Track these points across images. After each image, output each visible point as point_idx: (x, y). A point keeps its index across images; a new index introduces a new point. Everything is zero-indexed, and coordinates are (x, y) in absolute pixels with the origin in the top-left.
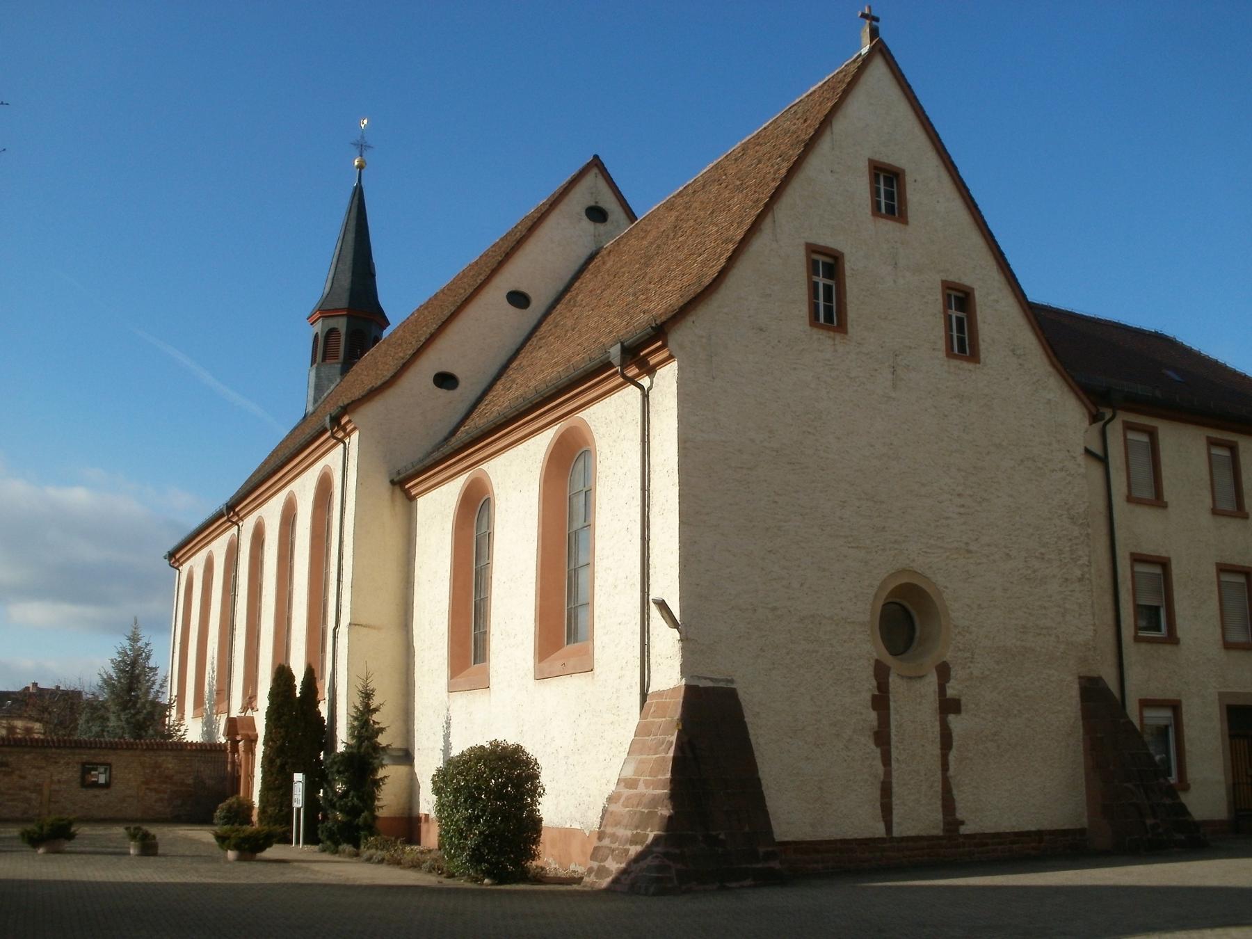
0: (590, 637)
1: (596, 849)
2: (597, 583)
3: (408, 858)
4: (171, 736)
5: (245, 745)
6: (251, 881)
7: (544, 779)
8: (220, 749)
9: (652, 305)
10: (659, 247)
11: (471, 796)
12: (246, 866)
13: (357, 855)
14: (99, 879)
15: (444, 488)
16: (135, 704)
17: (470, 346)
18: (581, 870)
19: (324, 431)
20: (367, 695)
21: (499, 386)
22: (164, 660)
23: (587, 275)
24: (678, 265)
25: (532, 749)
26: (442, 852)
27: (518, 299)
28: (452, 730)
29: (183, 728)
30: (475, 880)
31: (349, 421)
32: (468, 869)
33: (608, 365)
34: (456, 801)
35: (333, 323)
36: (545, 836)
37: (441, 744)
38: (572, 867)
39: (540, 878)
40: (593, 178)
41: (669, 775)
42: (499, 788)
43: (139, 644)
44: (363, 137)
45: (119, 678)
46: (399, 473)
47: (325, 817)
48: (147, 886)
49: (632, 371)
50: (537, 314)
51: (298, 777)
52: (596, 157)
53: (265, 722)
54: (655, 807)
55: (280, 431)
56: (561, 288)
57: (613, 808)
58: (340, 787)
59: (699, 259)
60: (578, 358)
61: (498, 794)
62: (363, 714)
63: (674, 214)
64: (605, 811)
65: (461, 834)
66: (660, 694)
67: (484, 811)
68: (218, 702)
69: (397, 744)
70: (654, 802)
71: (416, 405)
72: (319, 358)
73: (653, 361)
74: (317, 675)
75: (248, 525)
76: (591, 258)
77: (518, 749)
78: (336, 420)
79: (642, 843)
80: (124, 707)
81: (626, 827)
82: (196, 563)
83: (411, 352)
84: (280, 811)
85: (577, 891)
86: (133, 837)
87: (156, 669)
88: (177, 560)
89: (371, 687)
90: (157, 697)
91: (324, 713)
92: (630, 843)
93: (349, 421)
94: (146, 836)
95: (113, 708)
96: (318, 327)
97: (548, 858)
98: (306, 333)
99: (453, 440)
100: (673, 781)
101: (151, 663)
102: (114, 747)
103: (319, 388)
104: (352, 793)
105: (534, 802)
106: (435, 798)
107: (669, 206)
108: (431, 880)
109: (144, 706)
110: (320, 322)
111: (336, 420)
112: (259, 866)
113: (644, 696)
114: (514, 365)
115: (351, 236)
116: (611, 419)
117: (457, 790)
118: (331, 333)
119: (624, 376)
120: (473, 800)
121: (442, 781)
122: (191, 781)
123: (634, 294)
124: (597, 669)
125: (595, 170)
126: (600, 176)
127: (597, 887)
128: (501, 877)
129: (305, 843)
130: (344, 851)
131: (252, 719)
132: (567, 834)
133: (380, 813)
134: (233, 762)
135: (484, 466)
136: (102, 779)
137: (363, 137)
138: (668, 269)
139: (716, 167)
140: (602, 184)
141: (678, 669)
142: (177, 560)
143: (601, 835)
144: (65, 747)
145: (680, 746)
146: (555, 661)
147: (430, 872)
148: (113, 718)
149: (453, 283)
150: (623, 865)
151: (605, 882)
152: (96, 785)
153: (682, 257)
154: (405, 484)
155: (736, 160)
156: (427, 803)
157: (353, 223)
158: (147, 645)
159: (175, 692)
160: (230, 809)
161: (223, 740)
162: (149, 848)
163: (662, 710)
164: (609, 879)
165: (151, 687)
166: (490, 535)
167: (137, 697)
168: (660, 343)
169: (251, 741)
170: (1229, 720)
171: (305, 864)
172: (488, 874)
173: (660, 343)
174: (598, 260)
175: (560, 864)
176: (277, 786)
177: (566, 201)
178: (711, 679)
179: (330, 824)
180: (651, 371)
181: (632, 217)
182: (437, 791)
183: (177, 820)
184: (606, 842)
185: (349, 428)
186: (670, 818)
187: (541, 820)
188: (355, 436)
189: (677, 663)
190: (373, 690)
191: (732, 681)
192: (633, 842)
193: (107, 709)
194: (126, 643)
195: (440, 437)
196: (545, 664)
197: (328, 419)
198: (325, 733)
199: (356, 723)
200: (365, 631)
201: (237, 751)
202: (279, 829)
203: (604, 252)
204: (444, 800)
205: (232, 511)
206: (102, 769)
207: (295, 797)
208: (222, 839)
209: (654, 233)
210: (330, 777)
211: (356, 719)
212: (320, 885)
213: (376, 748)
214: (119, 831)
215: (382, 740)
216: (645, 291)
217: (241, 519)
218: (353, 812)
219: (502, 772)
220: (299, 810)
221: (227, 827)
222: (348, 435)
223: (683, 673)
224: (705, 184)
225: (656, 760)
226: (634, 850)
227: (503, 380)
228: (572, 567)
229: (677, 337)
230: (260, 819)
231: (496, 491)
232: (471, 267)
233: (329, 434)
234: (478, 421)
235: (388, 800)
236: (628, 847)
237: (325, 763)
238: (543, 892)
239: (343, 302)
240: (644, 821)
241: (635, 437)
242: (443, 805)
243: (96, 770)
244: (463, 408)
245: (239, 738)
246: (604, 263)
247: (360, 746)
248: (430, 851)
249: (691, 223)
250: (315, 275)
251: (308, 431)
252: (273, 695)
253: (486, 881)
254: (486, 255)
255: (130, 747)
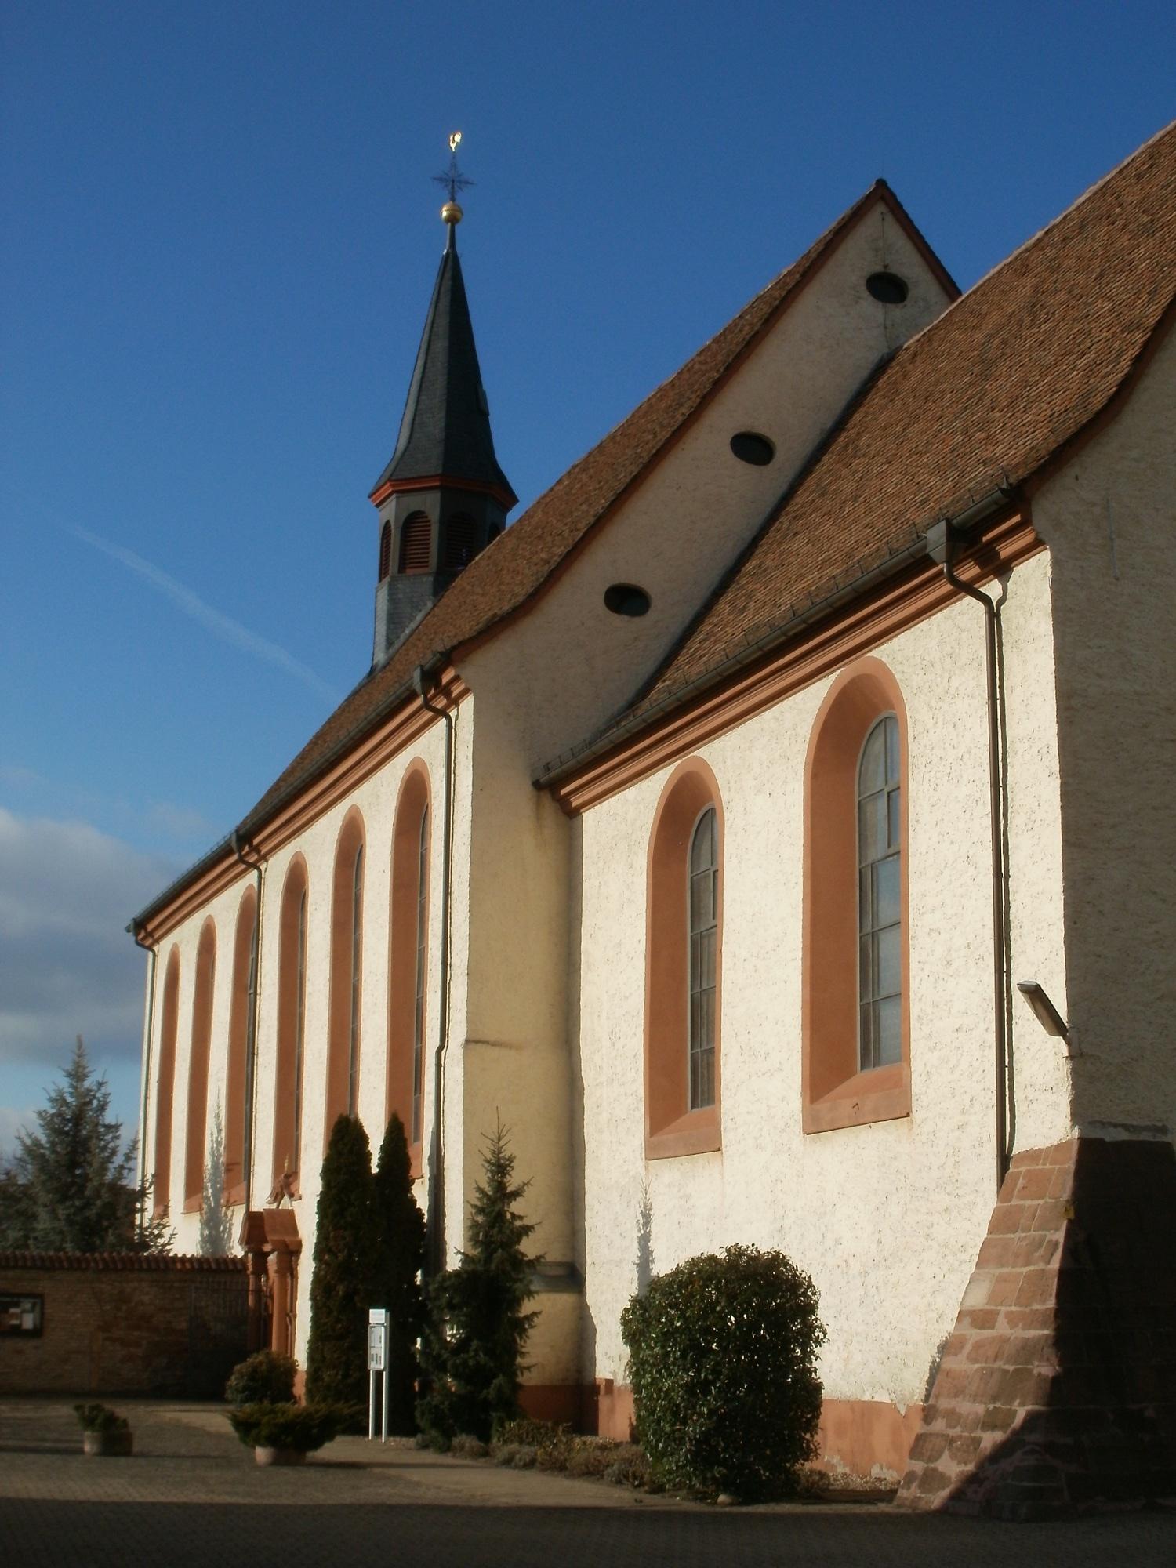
0: (903, 1056)
1: (920, 1438)
2: (914, 957)
3: (579, 1458)
4: (147, 1247)
5: (279, 1261)
6: (301, 1501)
7: (824, 1314)
8: (234, 1267)
9: (999, 450)
10: (1004, 342)
11: (694, 1345)
12: (289, 1474)
13: (486, 1454)
14: (35, 1495)
15: (631, 793)
16: (82, 1188)
17: (667, 536)
18: (891, 1476)
19: (411, 697)
20: (500, 1168)
21: (723, 606)
22: (132, 1114)
23: (875, 399)
24: (1043, 376)
25: (803, 1260)
26: (641, 1447)
27: (752, 448)
28: (654, 1228)
29: (167, 1232)
30: (702, 1497)
31: (456, 679)
32: (688, 1476)
33: (923, 562)
34: (667, 1354)
35: (415, 502)
36: (827, 1418)
37: (634, 1253)
38: (876, 1471)
39: (819, 1491)
40: (877, 222)
41: (1051, 1303)
42: (742, 1326)
43: (87, 1084)
44: (454, 166)
45: (53, 1144)
46: (547, 768)
47: (426, 1387)
48: (120, 1509)
49: (968, 571)
50: (790, 473)
51: (378, 1316)
52: (881, 184)
53: (315, 1219)
54: (1028, 1361)
55: (326, 694)
56: (829, 425)
57: (950, 1363)
58: (451, 1333)
59: (1081, 363)
60: (866, 551)
61: (742, 1339)
62: (492, 1201)
63: (1029, 281)
64: (935, 1369)
65: (675, 1414)
66: (1033, 1155)
67: (716, 1372)
68: (229, 1185)
69: (555, 1254)
70: (1027, 1351)
71: (575, 646)
72: (393, 566)
73: (1005, 551)
74: (409, 1133)
75: (277, 868)
76: (882, 367)
77: (777, 1261)
78: (431, 677)
79: (1003, 1427)
80: (64, 1195)
81: (975, 1398)
82: (185, 938)
83: (561, 550)
84: (346, 1376)
85: (888, 1515)
86: (89, 1422)
87: (116, 1127)
88: (150, 934)
89: (507, 1153)
90: (120, 1176)
91: (423, 1202)
92: (979, 1430)
93: (456, 679)
94: (111, 1420)
95: (44, 1197)
96: (389, 511)
97: (833, 1456)
98: (365, 523)
99: (646, 704)
100: (1060, 1312)
101: (109, 1118)
102: (48, 1266)
103: (395, 620)
104: (475, 1344)
105: (807, 1355)
106: (626, 1351)
107: (1021, 267)
108: (621, 1497)
109: (97, 1194)
110: (392, 503)
111: (431, 677)
112: (311, 1474)
113: (1004, 1159)
114: (750, 566)
115: (441, 345)
116: (931, 659)
117: (666, 1336)
118: (412, 522)
119: (953, 580)
120: (695, 1352)
121: (640, 1321)
122: (184, 1325)
123: (965, 432)
124: (918, 1114)
125: (880, 208)
126: (890, 218)
127: (923, 1506)
128: (748, 1491)
129: (391, 1432)
130: (462, 1448)
131: (290, 1215)
132: (865, 1412)
133: (526, 1379)
134: (258, 1291)
135: (703, 752)
136: (28, 1321)
137: (454, 166)
138: (1024, 383)
139: (1102, 192)
140: (894, 233)
141: (1065, 1109)
142: (150, 934)
143: (928, 1413)
144: (16, 1267)
145: (1072, 1250)
146: (841, 1099)
147: (619, 1482)
148: (43, 1214)
149: (630, 423)
150: (970, 1468)
151: (937, 1499)
152: (17, 1332)
153: (1050, 359)
154: (559, 786)
155: (1139, 177)
156: (612, 1358)
157: (444, 322)
158: (100, 1085)
159: (151, 1169)
160: (254, 1374)
161: (238, 1251)
162: (116, 1441)
163: (1037, 1183)
164: (945, 1493)
165: (109, 1160)
166: (716, 876)
167: (86, 1178)
168: (1017, 519)
169: (290, 1252)
170: (651, 1118)
171: (389, 1468)
172: (724, 1485)
173: (1017, 519)
174: (894, 370)
175: (854, 1466)
176: (339, 1332)
177: (831, 264)
178: (1126, 1127)
179: (436, 1399)
180: (1003, 570)
181: (951, 290)
182: (633, 1335)
183: (162, 1393)
184: (939, 1425)
185: (456, 690)
186: (1055, 1381)
187: (819, 1387)
188: (467, 705)
189: (1063, 1099)
190: (511, 1159)
191: (1163, 1130)
192: (989, 1424)
193: (33, 1200)
194: (64, 1084)
195: (621, 702)
196: (823, 1106)
197: (417, 675)
198: (425, 1238)
199: (480, 1219)
200: (493, 1052)
201: (266, 1271)
202: (344, 1408)
203: (903, 357)
204: (645, 1354)
205: (246, 845)
206: (28, 1306)
207: (372, 1351)
208: (246, 1428)
209: (995, 318)
210: (435, 1316)
211: (481, 1210)
212: (423, 1507)
213: (518, 1262)
214: (63, 1412)
215: (528, 1247)
216: (985, 424)
217: (264, 858)
218: (475, 1377)
219: (750, 1304)
220: (379, 1374)
221: (248, 1407)
222: (455, 702)
223: (1076, 1116)
224: (1082, 223)
225: (1027, 1276)
226: (990, 1439)
227: (730, 595)
228: (868, 929)
229: (1048, 507)
230: (310, 1392)
231: (725, 796)
232: (662, 392)
233: (419, 702)
234: (691, 669)
235: (539, 1353)
236: (978, 1433)
237: (431, 1290)
238: (826, 1518)
239: (432, 464)
240: (1007, 1386)
241: (977, 691)
242: (643, 1363)
243: (17, 1305)
244: (659, 648)
245: (267, 1248)
246: (905, 377)
247: (488, 1259)
248: (617, 1445)
249: (1062, 296)
250: (378, 416)
251: (381, 698)
252: (330, 1172)
253: (722, 1498)
254: (688, 369)
255: (75, 1265)
